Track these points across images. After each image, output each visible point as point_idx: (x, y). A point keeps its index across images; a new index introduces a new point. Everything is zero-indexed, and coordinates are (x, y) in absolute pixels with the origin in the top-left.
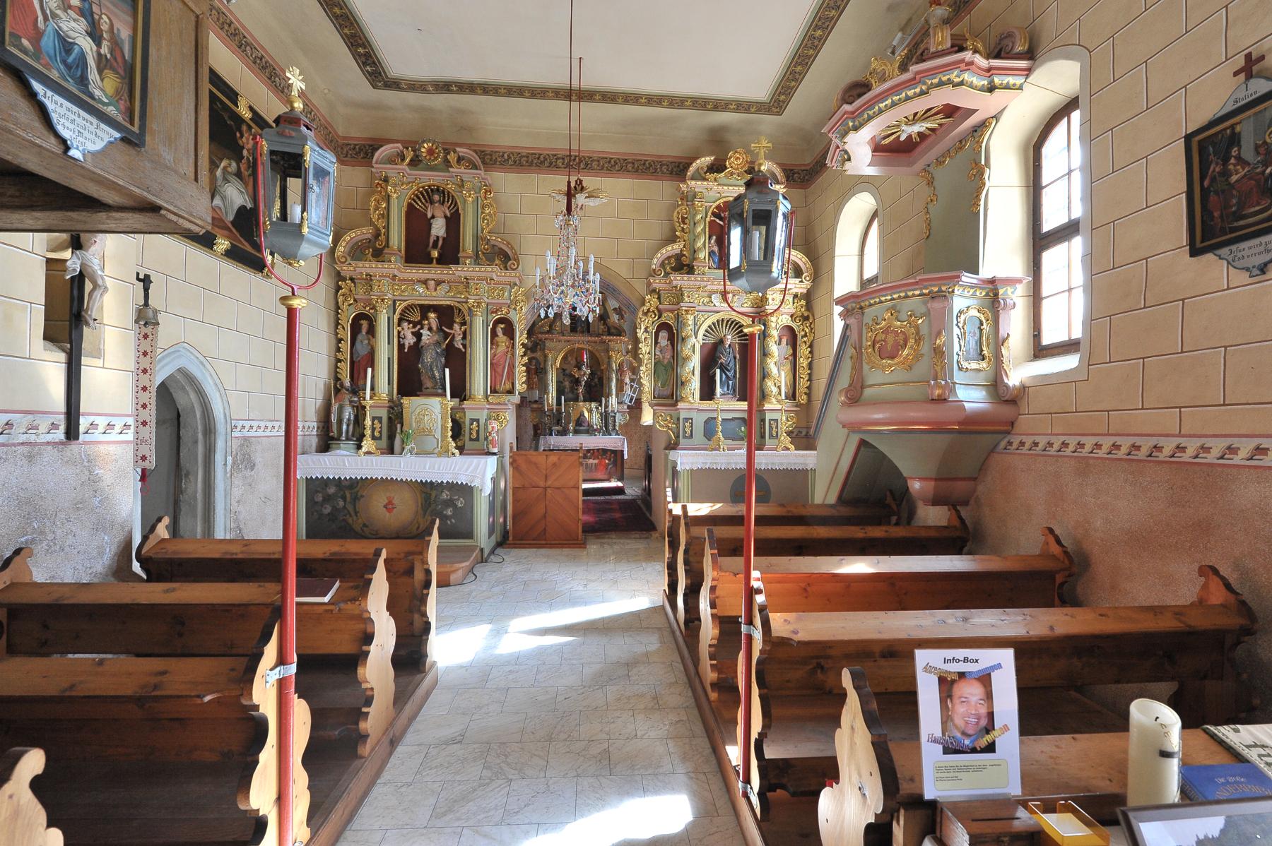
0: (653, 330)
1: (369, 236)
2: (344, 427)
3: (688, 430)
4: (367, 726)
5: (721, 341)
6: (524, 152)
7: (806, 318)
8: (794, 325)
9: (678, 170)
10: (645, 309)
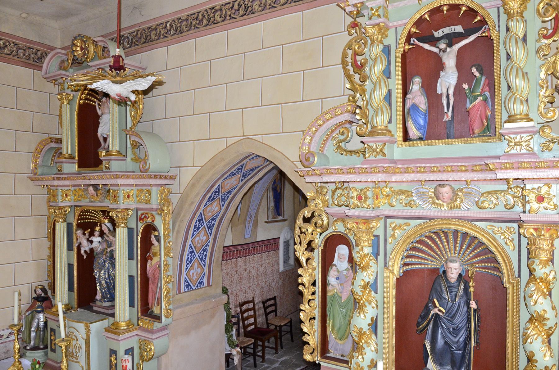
6: (184, 15)
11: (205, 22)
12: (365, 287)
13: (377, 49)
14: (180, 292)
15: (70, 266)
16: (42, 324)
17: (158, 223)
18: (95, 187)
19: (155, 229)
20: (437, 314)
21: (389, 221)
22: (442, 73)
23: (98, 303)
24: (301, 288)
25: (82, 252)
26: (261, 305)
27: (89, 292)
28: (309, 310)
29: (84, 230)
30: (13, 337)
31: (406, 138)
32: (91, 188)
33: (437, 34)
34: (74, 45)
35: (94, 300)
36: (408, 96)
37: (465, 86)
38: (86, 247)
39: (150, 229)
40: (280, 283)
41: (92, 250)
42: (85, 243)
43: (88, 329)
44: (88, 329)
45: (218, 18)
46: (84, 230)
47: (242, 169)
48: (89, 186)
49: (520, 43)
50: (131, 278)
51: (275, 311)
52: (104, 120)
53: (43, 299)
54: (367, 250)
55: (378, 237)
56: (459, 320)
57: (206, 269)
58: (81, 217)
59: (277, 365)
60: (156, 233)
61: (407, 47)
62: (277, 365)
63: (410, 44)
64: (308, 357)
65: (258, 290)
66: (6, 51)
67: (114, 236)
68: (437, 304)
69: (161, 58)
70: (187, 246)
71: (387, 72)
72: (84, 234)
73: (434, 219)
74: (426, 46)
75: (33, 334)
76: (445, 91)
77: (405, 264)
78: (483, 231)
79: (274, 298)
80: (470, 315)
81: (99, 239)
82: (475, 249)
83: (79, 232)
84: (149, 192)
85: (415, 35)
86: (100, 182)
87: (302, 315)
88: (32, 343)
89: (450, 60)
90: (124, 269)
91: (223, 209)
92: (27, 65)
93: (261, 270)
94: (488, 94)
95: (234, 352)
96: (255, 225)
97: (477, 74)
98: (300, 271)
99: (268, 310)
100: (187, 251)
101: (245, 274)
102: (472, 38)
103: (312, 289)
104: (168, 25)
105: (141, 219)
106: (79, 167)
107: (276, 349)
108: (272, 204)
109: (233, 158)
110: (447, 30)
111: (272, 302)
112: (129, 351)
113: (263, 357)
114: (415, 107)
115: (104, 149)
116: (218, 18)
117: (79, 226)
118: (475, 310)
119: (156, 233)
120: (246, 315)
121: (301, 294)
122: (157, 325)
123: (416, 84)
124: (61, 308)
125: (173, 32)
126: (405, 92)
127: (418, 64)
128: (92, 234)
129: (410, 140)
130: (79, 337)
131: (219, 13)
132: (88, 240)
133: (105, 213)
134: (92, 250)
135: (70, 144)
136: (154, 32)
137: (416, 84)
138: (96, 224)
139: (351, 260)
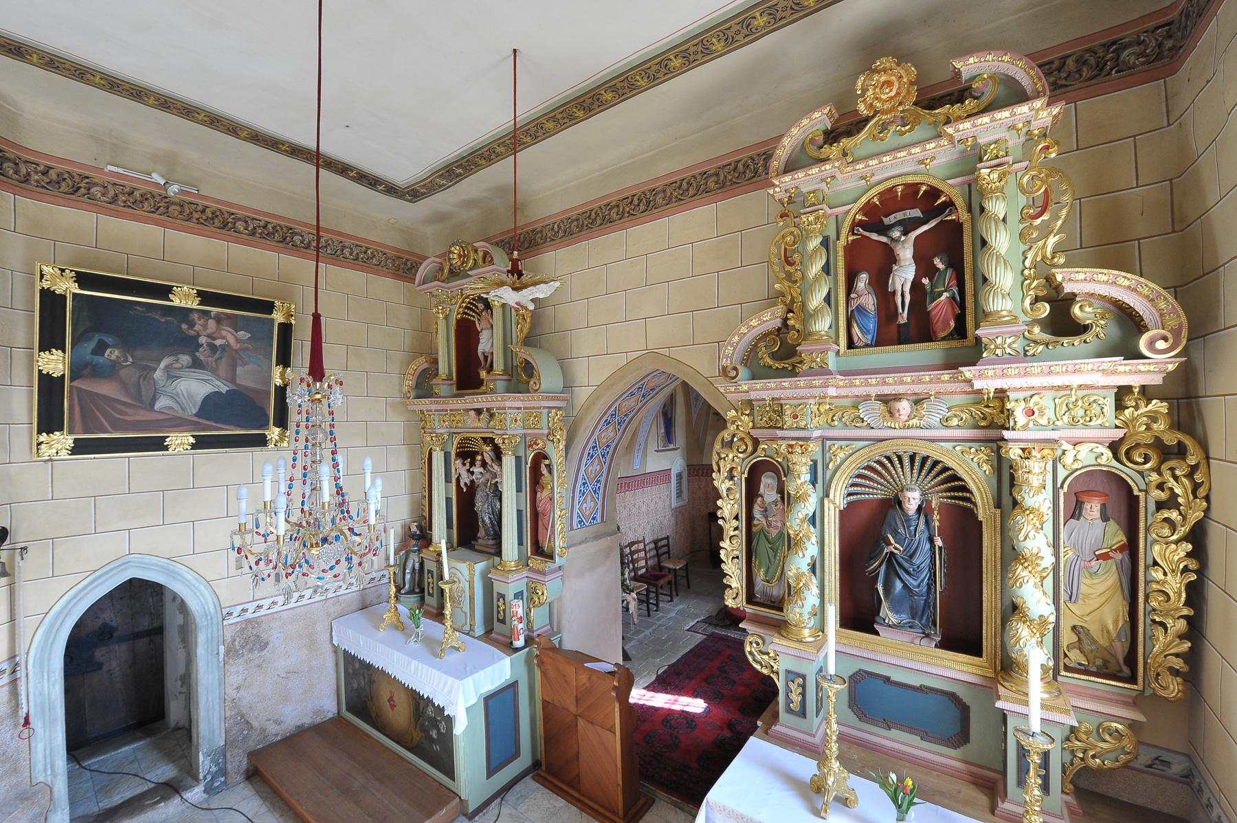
0: (742, 476)
1: (426, 366)
2: (408, 577)
3: (796, 698)
4: (980, 518)
5: (896, 502)
6: (574, 214)
7: (1180, 451)
8: (1127, 472)
9: (744, 172)
10: (727, 437)
11: (599, 221)
12: (802, 521)
13: (814, 243)
14: (572, 529)
15: (448, 500)
16: (417, 565)
17: (550, 450)
18: (479, 412)
19: (546, 458)
20: (892, 553)
21: (828, 443)
22: (895, 267)
23: (480, 541)
24: (721, 522)
25: (462, 484)
26: (652, 546)
27: (473, 531)
28: (731, 549)
29: (464, 459)
30: (385, 580)
31: (851, 345)
32: (472, 413)
33: (892, 219)
34: (451, 252)
35: (475, 538)
36: (853, 296)
37: (925, 281)
38: (465, 479)
39: (540, 457)
40: (673, 520)
41: (472, 482)
42: (464, 475)
43: (471, 571)
44: (471, 571)
45: (614, 216)
46: (464, 459)
47: (642, 390)
48: (468, 410)
49: (1001, 225)
50: (519, 512)
51: (668, 552)
52: (484, 337)
53: (420, 536)
54: (806, 477)
55: (815, 463)
56: (922, 558)
57: (600, 503)
58: (461, 445)
59: (673, 614)
60: (547, 462)
61: (850, 238)
62: (673, 614)
63: (853, 234)
64: (729, 602)
65: (648, 529)
66: (374, 261)
67: (501, 465)
68: (892, 541)
69: (555, 259)
70: (580, 477)
71: (827, 269)
72: (464, 464)
73: (882, 440)
74: (874, 236)
75: (408, 577)
76: (899, 288)
77: (850, 495)
78: (934, 452)
79: (667, 538)
80: (934, 553)
81: (481, 470)
82: (938, 475)
83: (459, 462)
84: (538, 416)
85: (862, 224)
86: (484, 406)
87: (723, 556)
88: (407, 586)
89: (906, 253)
90: (511, 504)
91: (619, 434)
92: (396, 276)
93: (652, 505)
94: (955, 290)
95: (629, 598)
96: (645, 455)
97: (941, 266)
98: (719, 503)
99: (661, 551)
100: (580, 482)
101: (634, 510)
102: (932, 224)
103: (735, 523)
104: (684, 183)
105: (531, 446)
106: (458, 389)
107: (671, 596)
108: (663, 430)
109: (633, 377)
110: (900, 216)
111: (664, 542)
112: (519, 595)
113: (657, 605)
114: (861, 309)
115: (484, 368)
116: (614, 216)
117: (458, 455)
118: (940, 548)
119: (547, 462)
120: (635, 556)
121: (721, 529)
122: (550, 565)
123: (863, 281)
124: (443, 546)
125: (561, 234)
126: (850, 288)
127: (866, 258)
128: (472, 464)
129: (856, 347)
130: (463, 580)
131: (615, 210)
132: (468, 471)
133: (489, 441)
134: (472, 482)
135: (446, 362)
136: (661, 195)
137: (863, 281)
138: (477, 453)
139: (781, 490)
